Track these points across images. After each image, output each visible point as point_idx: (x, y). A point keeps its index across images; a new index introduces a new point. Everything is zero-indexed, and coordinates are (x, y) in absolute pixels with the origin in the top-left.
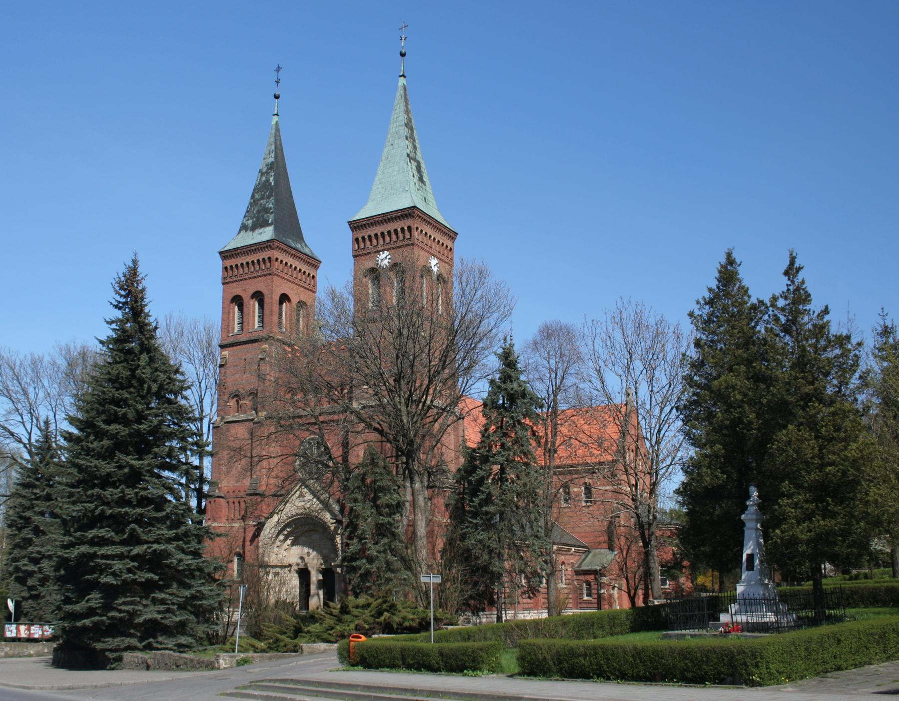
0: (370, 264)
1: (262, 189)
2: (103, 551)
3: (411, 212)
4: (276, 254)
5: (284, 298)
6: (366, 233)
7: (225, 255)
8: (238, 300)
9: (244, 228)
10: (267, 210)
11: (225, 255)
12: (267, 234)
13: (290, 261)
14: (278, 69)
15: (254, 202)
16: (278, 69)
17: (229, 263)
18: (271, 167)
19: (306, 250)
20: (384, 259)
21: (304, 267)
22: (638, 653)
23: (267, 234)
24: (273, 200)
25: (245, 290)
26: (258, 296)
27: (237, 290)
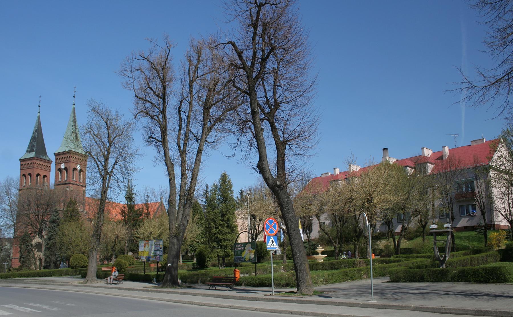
0: (59, 167)
1: (33, 139)
2: (180, 217)
3: (69, 152)
4: (35, 161)
5: (38, 175)
6: (58, 157)
7: (21, 160)
8: (24, 175)
9: (27, 151)
10: (34, 146)
11: (21, 160)
12: (33, 154)
13: (41, 163)
14: (40, 97)
15: (30, 143)
16: (40, 97)
17: (23, 163)
18: (36, 131)
19: (47, 158)
20: (63, 166)
21: (46, 164)
22: (297, 300)
23: (33, 154)
24: (37, 143)
25: (27, 172)
26: (30, 174)
27: (24, 173)
